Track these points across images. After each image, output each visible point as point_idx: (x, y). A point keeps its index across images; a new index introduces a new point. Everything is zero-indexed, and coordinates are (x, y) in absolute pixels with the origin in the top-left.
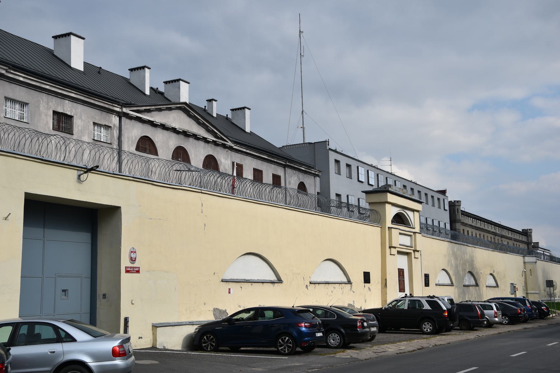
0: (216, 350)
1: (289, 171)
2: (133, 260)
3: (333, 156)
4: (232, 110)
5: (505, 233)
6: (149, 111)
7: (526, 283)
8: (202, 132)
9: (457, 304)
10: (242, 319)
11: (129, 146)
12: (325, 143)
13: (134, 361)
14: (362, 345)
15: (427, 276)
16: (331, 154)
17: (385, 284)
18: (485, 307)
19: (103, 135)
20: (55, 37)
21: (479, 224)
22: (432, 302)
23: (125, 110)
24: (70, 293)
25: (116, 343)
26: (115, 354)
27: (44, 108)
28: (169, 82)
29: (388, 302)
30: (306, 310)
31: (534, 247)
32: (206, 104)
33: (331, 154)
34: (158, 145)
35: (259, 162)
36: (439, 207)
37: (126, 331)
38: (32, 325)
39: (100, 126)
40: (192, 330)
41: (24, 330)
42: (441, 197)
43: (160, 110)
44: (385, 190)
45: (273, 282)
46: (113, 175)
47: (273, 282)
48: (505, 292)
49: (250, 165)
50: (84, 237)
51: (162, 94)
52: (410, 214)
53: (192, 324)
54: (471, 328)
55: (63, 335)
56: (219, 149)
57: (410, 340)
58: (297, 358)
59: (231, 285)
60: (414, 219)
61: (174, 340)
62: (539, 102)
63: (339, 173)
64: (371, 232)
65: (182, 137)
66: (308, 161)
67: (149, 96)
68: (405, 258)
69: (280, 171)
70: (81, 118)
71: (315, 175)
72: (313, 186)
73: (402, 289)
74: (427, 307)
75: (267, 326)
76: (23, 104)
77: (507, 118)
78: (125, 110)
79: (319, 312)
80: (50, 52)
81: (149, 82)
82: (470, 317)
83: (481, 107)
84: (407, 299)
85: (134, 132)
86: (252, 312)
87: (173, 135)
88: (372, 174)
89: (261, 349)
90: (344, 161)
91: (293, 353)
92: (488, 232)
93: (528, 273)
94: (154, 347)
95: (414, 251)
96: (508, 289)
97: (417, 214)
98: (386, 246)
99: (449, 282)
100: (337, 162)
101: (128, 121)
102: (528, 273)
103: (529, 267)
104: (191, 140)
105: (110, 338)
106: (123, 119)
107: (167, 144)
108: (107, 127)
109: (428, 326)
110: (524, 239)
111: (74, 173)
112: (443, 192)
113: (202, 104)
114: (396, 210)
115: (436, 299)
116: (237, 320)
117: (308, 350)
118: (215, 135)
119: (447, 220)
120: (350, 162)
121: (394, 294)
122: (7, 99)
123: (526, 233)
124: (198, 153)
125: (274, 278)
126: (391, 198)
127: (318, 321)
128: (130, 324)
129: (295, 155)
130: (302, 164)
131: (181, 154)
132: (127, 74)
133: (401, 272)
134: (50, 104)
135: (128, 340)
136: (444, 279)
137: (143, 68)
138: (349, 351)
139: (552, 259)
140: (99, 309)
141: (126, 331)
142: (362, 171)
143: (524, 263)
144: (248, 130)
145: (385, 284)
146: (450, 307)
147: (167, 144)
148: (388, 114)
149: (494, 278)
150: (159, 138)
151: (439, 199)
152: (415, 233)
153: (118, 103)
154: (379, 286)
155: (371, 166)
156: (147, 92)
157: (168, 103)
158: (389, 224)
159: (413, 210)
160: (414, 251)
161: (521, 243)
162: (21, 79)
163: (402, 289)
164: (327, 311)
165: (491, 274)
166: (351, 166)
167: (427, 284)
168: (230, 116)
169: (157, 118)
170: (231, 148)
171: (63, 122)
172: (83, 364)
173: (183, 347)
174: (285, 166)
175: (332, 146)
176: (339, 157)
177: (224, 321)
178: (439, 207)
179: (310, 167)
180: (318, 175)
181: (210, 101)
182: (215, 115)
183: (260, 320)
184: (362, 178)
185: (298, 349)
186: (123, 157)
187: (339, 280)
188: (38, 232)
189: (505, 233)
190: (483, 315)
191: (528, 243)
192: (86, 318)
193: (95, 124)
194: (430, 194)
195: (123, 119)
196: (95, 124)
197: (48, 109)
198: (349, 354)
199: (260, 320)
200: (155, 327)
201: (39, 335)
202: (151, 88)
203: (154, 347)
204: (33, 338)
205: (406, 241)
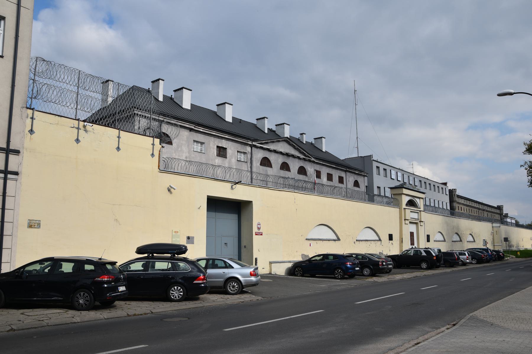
0: (302, 276)
1: (348, 174)
2: (259, 229)
3: (375, 164)
4: (315, 139)
5: (485, 208)
6: (267, 143)
7: (493, 239)
8: (297, 154)
9: (443, 253)
10: (316, 260)
11: (256, 164)
12: (370, 157)
13: (259, 279)
14: (383, 275)
15: (428, 236)
16: (374, 163)
17: (401, 241)
18: (461, 254)
19: (242, 157)
20: (218, 105)
21: (468, 203)
22: (427, 251)
23: (254, 143)
24: (228, 244)
25: (252, 270)
26: (251, 275)
27: (213, 143)
28: (278, 125)
29: (404, 250)
30: (351, 255)
31: (504, 216)
32: (299, 136)
33: (374, 163)
34: (272, 162)
35: (331, 169)
36: (443, 193)
37: (256, 264)
38: (214, 260)
39: (241, 152)
40: (290, 265)
41: (211, 262)
42: (444, 187)
43: (273, 142)
44: (401, 187)
45: (335, 240)
46: (248, 185)
47: (335, 240)
48: (480, 245)
49: (325, 171)
50: (235, 217)
51: (274, 131)
52: (418, 200)
53: (290, 262)
54: (452, 266)
55: (228, 265)
56: (307, 163)
57: (412, 272)
58: (345, 280)
59: (311, 242)
60: (420, 203)
61: (280, 270)
62: (512, 124)
63: (379, 174)
64: (394, 212)
65: (286, 156)
66: (360, 168)
67: (267, 134)
68: (415, 226)
69: (343, 174)
70: (231, 149)
71: (364, 176)
72: (363, 182)
73: (412, 243)
74: (424, 254)
75: (329, 264)
76: (202, 143)
77: (491, 134)
78: (254, 143)
79: (360, 257)
80: (215, 113)
81: (267, 125)
82: (451, 260)
83: (474, 127)
84: (413, 250)
85: (259, 155)
86: (322, 257)
87: (281, 156)
88: (399, 174)
89: (329, 276)
90: (382, 167)
91: (343, 278)
92: (475, 208)
93: (495, 233)
94: (270, 273)
95: (420, 222)
96: (482, 243)
97: (421, 200)
98: (403, 219)
99: (443, 239)
100: (378, 167)
101: (255, 149)
102: (495, 233)
103: (495, 229)
104: (291, 158)
105: (249, 267)
106: (253, 148)
107: (276, 160)
108: (245, 153)
109: (424, 265)
110: (498, 211)
111: (229, 185)
112: (445, 184)
113: (297, 136)
114: (408, 198)
115: (429, 250)
116: (314, 260)
117: (352, 276)
118: (305, 155)
119: (448, 201)
120: (386, 167)
121: (407, 246)
122: (194, 141)
123: (500, 208)
124: (295, 165)
125: (335, 238)
126: (405, 191)
127: (357, 261)
128: (258, 261)
129: (352, 165)
130: (356, 170)
131: (285, 167)
132: (255, 122)
133: (412, 234)
134: (215, 142)
135: (257, 268)
136: (439, 237)
137: (264, 118)
138: (374, 278)
139: (517, 225)
140: (243, 252)
141: (256, 264)
142: (393, 172)
143: (493, 227)
144: (324, 150)
145: (401, 241)
146: (437, 254)
147: (276, 160)
148: (414, 133)
149: (472, 236)
150: (273, 157)
151: (442, 188)
152: (420, 211)
153: (250, 139)
154: (398, 242)
155: (399, 169)
156: (266, 131)
157: (278, 137)
158: (404, 206)
159: (419, 198)
160: (420, 222)
161: (496, 215)
162: (201, 130)
163: (412, 243)
164: (364, 256)
165: (470, 234)
166: (387, 170)
167: (428, 240)
168: (313, 142)
169: (272, 147)
170: (314, 162)
171: (222, 152)
172: (237, 279)
173: (285, 274)
174: (346, 171)
175: (374, 158)
176: (379, 165)
177: (307, 261)
178: (443, 193)
179: (361, 171)
180: (366, 176)
181: (302, 134)
182: (304, 142)
183: (326, 260)
184: (394, 177)
185: (346, 276)
186: (253, 175)
187: (374, 239)
188: (213, 214)
189: (485, 208)
190: (459, 258)
191: (501, 214)
192: (236, 257)
193: (238, 151)
194: (436, 185)
195: (253, 148)
196: (238, 151)
197: (214, 145)
198: (375, 279)
199: (326, 260)
200: (271, 263)
201: (217, 265)
202: (268, 129)
203: (270, 273)
204: (215, 266)
205: (415, 216)
